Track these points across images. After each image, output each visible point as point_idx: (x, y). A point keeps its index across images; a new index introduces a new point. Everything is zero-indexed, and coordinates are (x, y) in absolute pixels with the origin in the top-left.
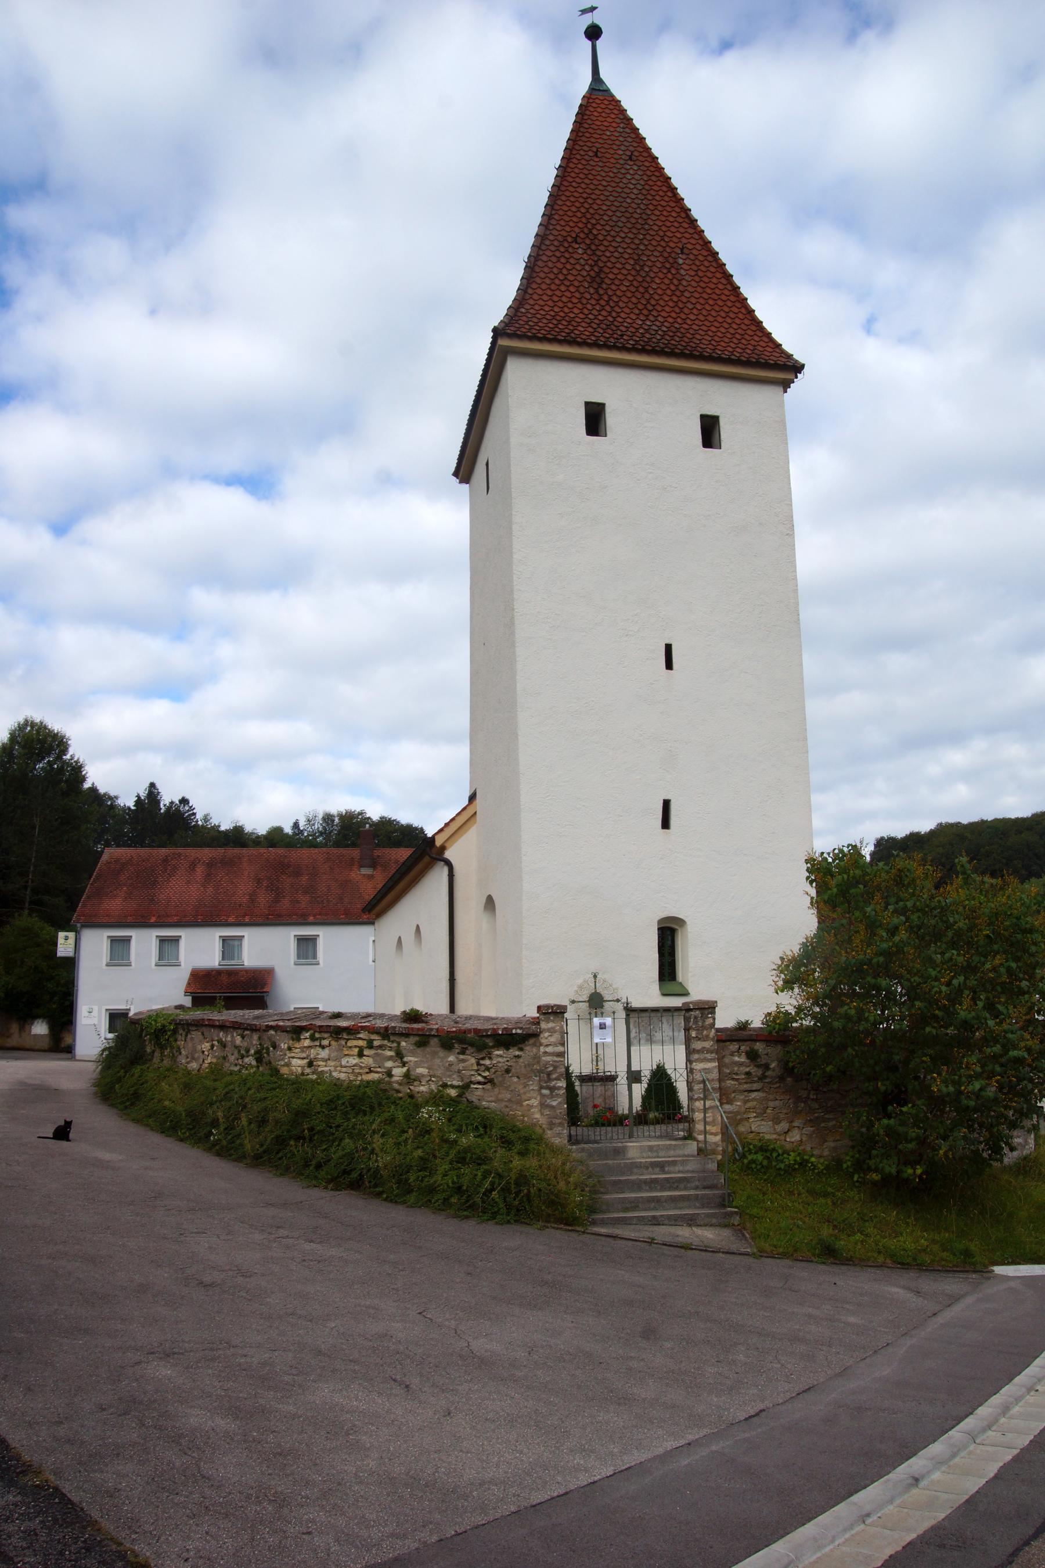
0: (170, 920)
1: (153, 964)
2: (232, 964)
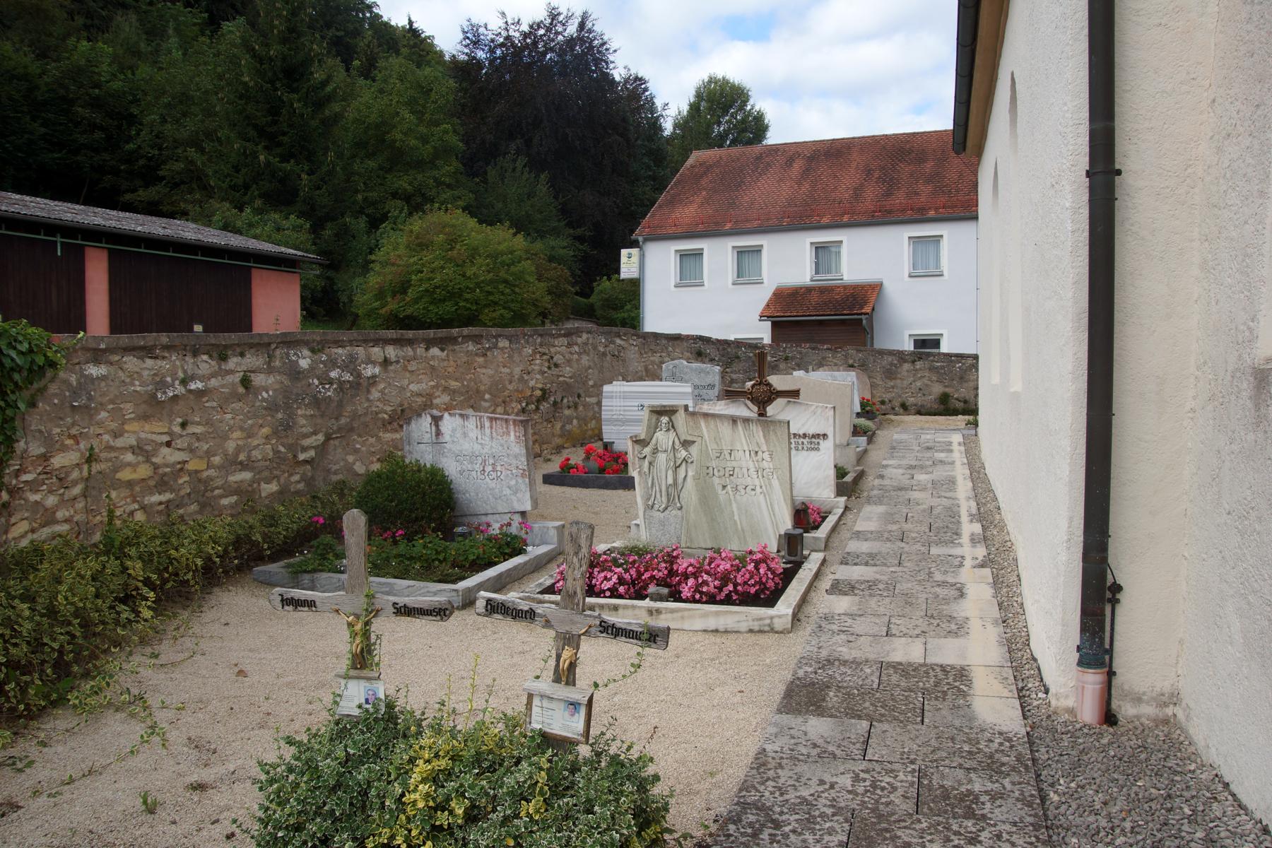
1: (730, 281)
2: (827, 279)
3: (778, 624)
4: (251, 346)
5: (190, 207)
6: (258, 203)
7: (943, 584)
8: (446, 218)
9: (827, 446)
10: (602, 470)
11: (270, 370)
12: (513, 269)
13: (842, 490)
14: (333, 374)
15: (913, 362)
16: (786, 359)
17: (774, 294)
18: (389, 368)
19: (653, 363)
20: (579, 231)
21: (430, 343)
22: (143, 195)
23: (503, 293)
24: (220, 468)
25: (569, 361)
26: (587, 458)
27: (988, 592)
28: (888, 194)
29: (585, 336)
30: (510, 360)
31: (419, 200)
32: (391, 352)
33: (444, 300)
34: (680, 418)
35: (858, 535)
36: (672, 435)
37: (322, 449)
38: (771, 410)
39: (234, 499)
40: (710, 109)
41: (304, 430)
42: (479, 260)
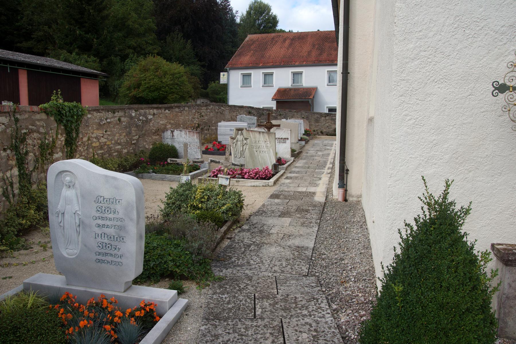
0: (268, 65)
1: (261, 86)
2: (297, 85)
3: (270, 184)
4: (121, 109)
5: (50, 52)
6: (77, 50)
7: (316, 177)
8: (154, 60)
9: (288, 142)
10: (219, 150)
11: (125, 117)
12: (180, 79)
13: (292, 156)
14: (141, 118)
15: (325, 117)
16: (280, 115)
17: (278, 91)
18: (155, 116)
19: (234, 116)
20: (203, 63)
21: (166, 109)
22: (25, 45)
23: (176, 89)
24: (114, 144)
25: (207, 115)
26: (214, 146)
27: (327, 179)
28: (320, 54)
29: (211, 106)
30: (187, 113)
31: (139, 49)
32: (155, 111)
33: (154, 91)
34: (244, 132)
35: (296, 167)
36: (242, 136)
37: (137, 140)
38: (272, 130)
39: (116, 153)
40: (255, 13)
41: (134, 134)
42: (167, 76)
